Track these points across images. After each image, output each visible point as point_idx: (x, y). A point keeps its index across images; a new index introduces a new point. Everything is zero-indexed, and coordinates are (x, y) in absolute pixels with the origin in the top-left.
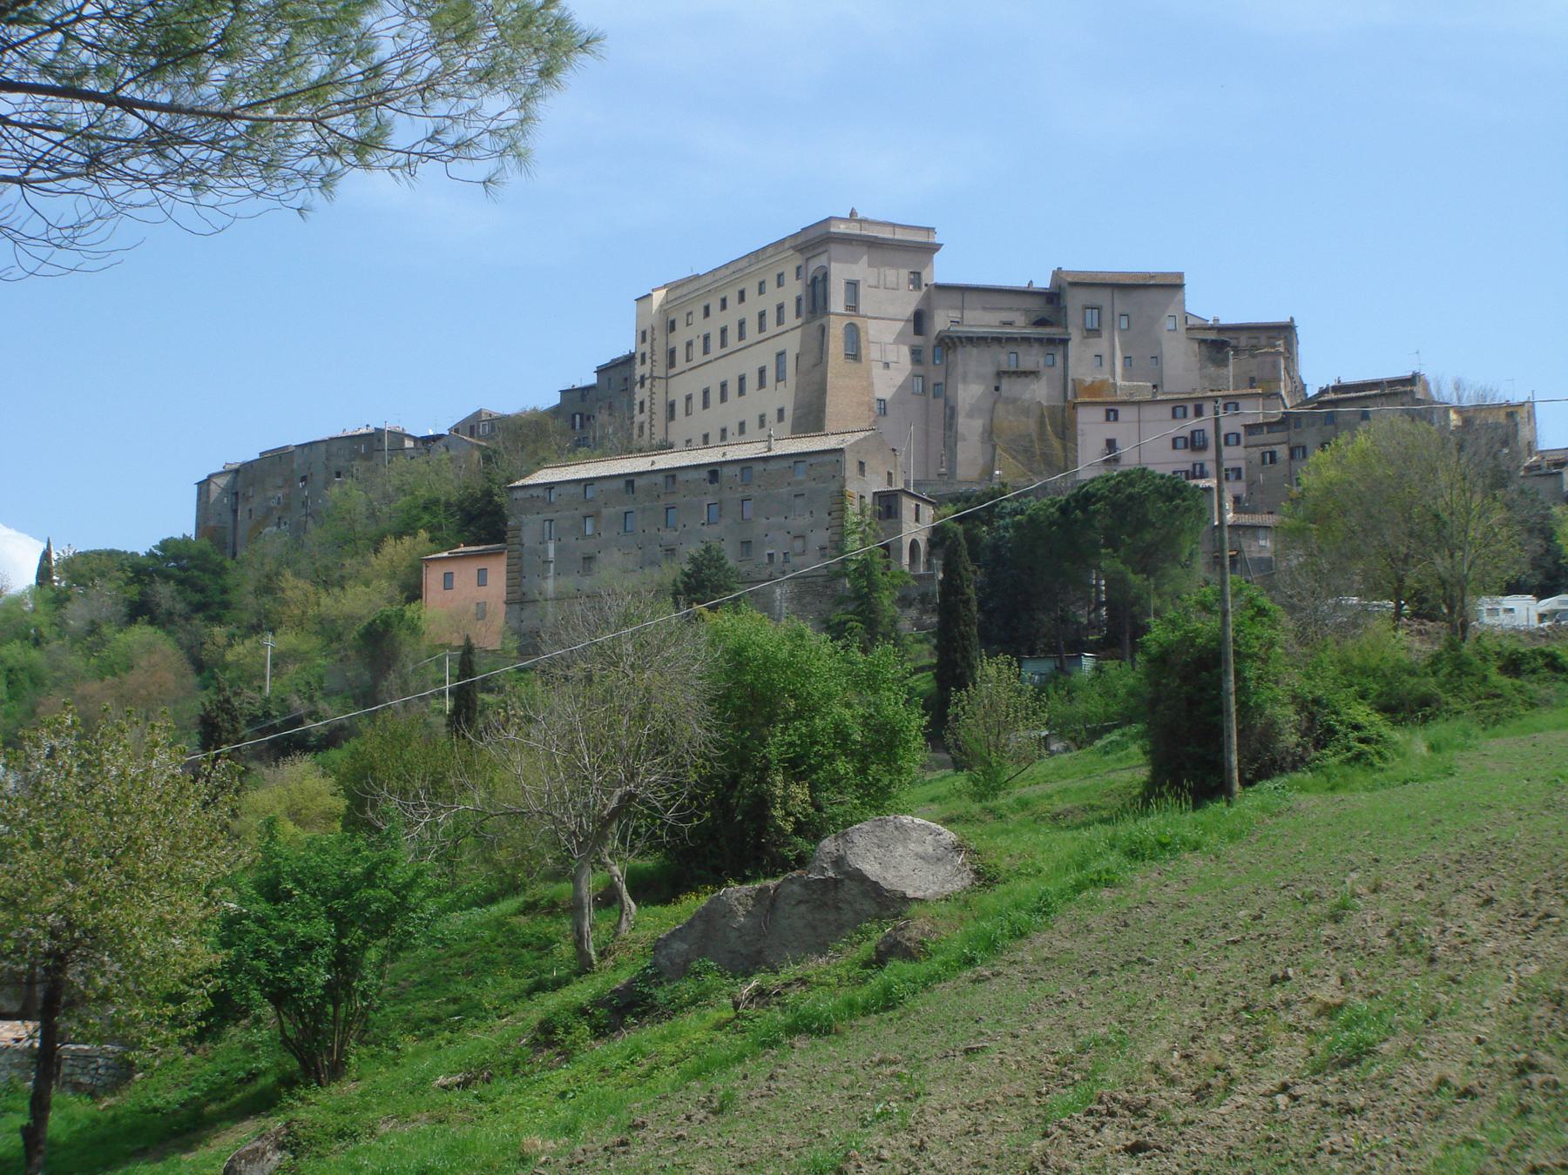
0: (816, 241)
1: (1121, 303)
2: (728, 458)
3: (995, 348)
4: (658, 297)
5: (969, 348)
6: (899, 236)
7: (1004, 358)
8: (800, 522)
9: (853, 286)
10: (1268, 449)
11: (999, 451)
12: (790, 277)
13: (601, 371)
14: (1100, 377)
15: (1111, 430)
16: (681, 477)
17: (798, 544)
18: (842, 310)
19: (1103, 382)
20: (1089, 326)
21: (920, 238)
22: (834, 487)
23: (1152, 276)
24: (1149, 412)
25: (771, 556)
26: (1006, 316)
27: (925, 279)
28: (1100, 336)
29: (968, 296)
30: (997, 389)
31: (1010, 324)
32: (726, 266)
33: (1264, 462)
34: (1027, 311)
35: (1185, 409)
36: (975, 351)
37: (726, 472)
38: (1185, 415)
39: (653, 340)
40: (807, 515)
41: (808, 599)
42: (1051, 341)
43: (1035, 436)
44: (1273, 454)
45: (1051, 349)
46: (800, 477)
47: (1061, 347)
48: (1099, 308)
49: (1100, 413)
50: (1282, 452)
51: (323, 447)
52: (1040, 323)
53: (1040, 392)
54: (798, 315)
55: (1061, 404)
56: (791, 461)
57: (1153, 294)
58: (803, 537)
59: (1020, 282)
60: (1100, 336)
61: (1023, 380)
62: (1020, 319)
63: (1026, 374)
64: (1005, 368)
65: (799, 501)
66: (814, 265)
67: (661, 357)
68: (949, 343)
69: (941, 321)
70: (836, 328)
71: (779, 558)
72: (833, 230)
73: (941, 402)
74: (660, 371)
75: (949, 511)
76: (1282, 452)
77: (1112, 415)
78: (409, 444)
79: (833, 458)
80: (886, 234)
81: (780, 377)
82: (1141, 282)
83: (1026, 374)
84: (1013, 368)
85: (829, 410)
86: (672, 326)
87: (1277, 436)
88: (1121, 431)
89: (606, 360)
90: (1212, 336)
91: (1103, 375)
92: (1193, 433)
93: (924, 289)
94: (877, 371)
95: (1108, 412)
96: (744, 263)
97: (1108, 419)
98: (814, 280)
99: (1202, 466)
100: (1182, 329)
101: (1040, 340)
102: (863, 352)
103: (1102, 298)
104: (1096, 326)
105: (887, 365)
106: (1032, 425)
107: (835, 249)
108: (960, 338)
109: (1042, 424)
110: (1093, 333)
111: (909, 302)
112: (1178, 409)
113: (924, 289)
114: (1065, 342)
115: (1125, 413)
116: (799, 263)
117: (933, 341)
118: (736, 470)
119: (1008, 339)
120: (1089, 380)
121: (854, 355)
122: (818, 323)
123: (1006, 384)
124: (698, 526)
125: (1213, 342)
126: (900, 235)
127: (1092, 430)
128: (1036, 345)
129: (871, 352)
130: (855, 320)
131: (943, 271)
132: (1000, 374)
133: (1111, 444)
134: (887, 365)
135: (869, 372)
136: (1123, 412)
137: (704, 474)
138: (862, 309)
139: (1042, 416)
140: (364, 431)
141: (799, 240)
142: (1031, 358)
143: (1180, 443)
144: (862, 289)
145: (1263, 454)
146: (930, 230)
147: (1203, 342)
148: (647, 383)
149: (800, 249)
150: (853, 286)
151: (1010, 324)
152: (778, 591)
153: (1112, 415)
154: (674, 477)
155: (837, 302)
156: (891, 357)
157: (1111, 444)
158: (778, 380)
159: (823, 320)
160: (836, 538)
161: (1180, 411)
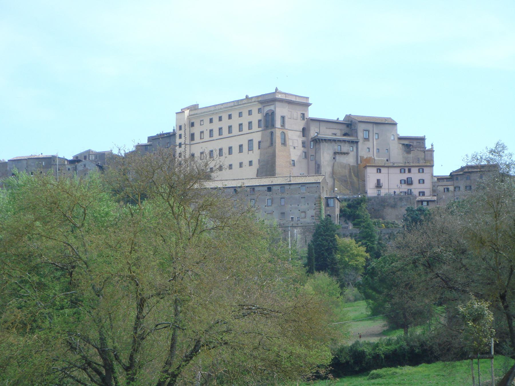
0: (268, 101)
1: (376, 129)
2: (274, 183)
3: (333, 143)
4: (187, 112)
5: (324, 143)
6: (297, 100)
7: (336, 147)
8: (303, 207)
9: (283, 118)
10: (446, 187)
11: (336, 181)
12: (255, 111)
13: (150, 139)
14: (369, 156)
15: (379, 176)
16: (256, 189)
17: (303, 215)
18: (280, 127)
19: (370, 158)
20: (365, 137)
21: (304, 101)
22: (316, 195)
23: (386, 119)
24: (392, 170)
25: (292, 218)
26: (334, 131)
27: (306, 116)
28: (369, 141)
29: (321, 123)
30: (334, 158)
31: (335, 134)
32: (222, 104)
33: (445, 191)
34: (341, 130)
35: (405, 170)
36: (327, 144)
37: (274, 188)
38: (405, 172)
39: (185, 130)
40: (306, 205)
41: (307, 234)
42: (352, 142)
43: (348, 176)
44: (448, 189)
45: (352, 145)
46: (302, 191)
47: (355, 144)
48: (369, 131)
49: (374, 170)
50: (451, 188)
51: (25, 162)
52: (345, 135)
53: (350, 160)
54: (259, 126)
55: (355, 165)
56: (300, 186)
57: (387, 127)
58: (305, 212)
59: (334, 118)
60: (369, 141)
61: (343, 156)
62: (338, 132)
63: (344, 153)
64: (337, 151)
65: (303, 199)
66: (267, 109)
67: (188, 136)
68: (317, 141)
69: (313, 133)
70: (278, 133)
71: (295, 219)
72: (277, 97)
73: (314, 162)
74: (188, 142)
75: (345, 204)
76: (451, 188)
77: (379, 171)
78: (66, 162)
79: (318, 185)
80: (293, 99)
81: (250, 149)
82: (379, 122)
83: (344, 153)
84: (339, 151)
85: (277, 163)
86: (192, 125)
87: (449, 183)
88: (383, 177)
89: (154, 134)
90: (406, 142)
91: (370, 155)
92: (407, 178)
93: (306, 120)
94: (292, 149)
95: (377, 169)
96: (232, 104)
97: (377, 172)
98: (267, 114)
99: (411, 190)
100: (396, 139)
101: (349, 142)
102: (287, 143)
103: (370, 127)
104: (367, 137)
105: (295, 148)
106: (347, 171)
107: (277, 104)
108: (322, 139)
109: (350, 172)
110: (367, 139)
111: (301, 125)
112: (402, 170)
113: (306, 120)
114: (357, 142)
115: (383, 170)
116: (260, 107)
117: (310, 140)
118: (279, 187)
119: (338, 141)
120: (365, 157)
121: (284, 143)
122: (270, 131)
123: (338, 157)
124: (264, 207)
125: (407, 145)
126: (298, 100)
127: (371, 177)
128: (347, 143)
129: (289, 143)
130: (284, 131)
131: (313, 113)
132: (335, 153)
133: (378, 181)
134: (295, 148)
135: (289, 150)
136: (383, 170)
137: (266, 188)
138: (287, 126)
139: (350, 169)
140: (41, 156)
141: (260, 99)
142: (345, 148)
143: (403, 182)
144: (286, 119)
145: (444, 189)
146: (307, 98)
147: (403, 144)
148: (183, 146)
149: (261, 102)
150: (283, 118)
151: (335, 134)
152: (296, 230)
153: (379, 171)
154: (254, 189)
155: (278, 124)
156: (296, 145)
157: (378, 181)
158: (249, 150)
159: (273, 130)
160: (318, 213)
161: (403, 170)
